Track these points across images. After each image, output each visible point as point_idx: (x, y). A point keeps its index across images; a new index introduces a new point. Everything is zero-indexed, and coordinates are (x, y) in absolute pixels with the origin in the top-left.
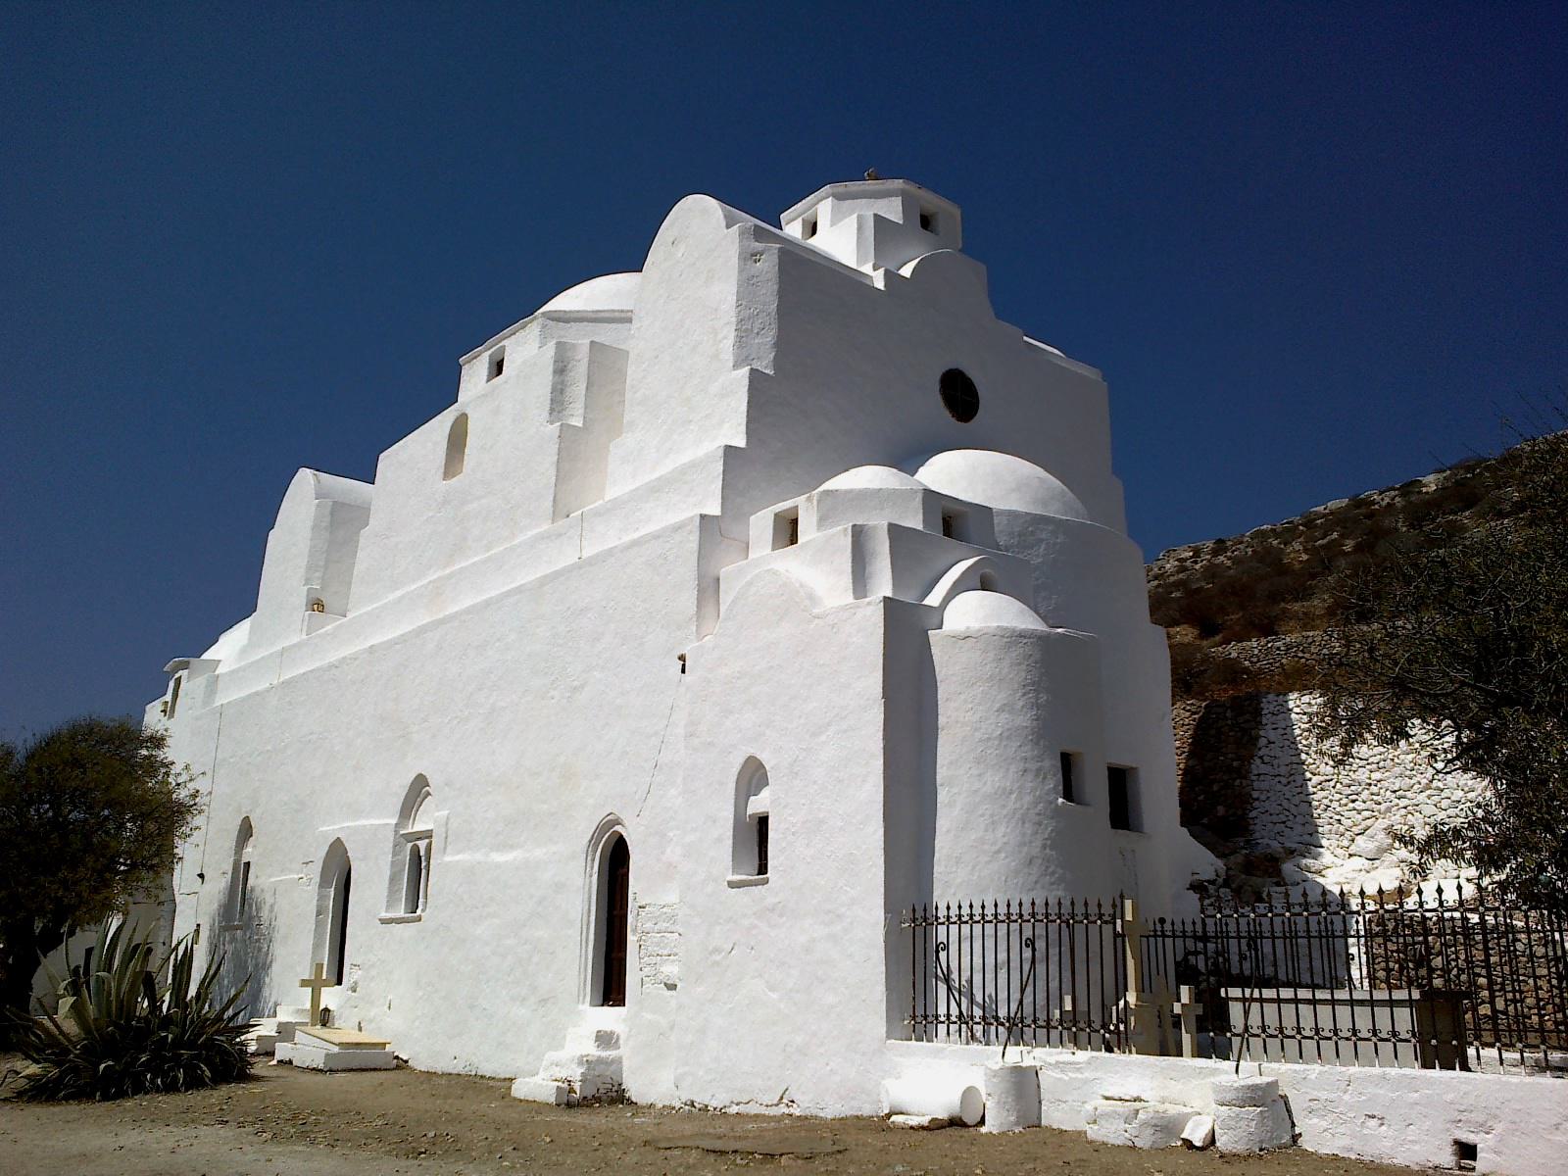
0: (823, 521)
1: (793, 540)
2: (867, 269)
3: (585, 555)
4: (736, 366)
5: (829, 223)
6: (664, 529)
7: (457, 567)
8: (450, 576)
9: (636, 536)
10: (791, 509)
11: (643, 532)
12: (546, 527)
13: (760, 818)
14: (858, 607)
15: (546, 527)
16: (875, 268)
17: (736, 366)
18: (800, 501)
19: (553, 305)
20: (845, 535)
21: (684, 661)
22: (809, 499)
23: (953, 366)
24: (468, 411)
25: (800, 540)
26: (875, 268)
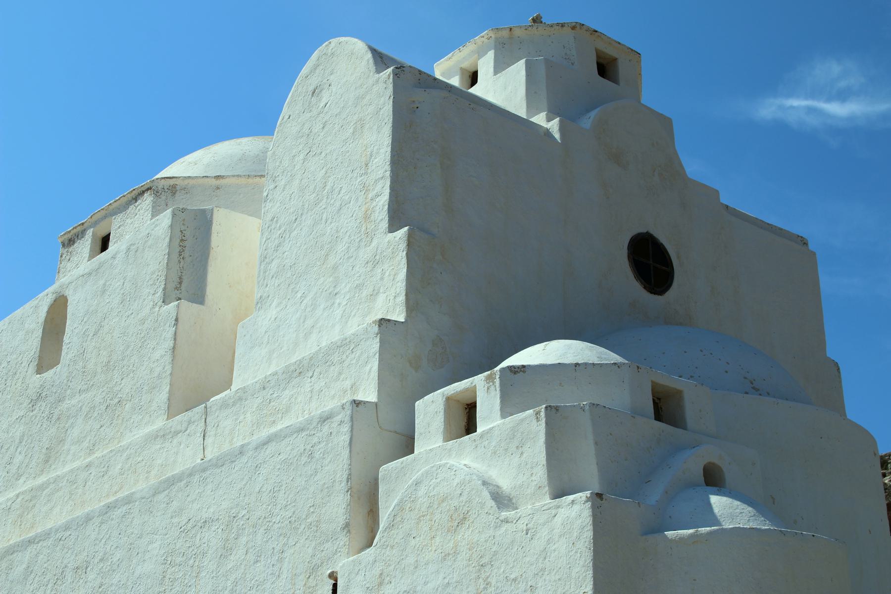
0: (508, 407)
1: (470, 427)
2: (540, 119)
3: (209, 456)
4: (393, 228)
5: (492, 70)
6: (309, 421)
7: (53, 475)
8: (42, 487)
9: (273, 430)
10: (466, 390)
11: (279, 427)
12: (160, 423)
13: (468, 405)
14: (559, 507)
15: (160, 423)
16: (549, 120)
17: (393, 228)
18: (479, 380)
19: (378, 354)
20: (538, 419)
21: (336, 580)
22: (490, 379)
23: (643, 230)
24: (69, 293)
25: (480, 429)
26: (549, 120)
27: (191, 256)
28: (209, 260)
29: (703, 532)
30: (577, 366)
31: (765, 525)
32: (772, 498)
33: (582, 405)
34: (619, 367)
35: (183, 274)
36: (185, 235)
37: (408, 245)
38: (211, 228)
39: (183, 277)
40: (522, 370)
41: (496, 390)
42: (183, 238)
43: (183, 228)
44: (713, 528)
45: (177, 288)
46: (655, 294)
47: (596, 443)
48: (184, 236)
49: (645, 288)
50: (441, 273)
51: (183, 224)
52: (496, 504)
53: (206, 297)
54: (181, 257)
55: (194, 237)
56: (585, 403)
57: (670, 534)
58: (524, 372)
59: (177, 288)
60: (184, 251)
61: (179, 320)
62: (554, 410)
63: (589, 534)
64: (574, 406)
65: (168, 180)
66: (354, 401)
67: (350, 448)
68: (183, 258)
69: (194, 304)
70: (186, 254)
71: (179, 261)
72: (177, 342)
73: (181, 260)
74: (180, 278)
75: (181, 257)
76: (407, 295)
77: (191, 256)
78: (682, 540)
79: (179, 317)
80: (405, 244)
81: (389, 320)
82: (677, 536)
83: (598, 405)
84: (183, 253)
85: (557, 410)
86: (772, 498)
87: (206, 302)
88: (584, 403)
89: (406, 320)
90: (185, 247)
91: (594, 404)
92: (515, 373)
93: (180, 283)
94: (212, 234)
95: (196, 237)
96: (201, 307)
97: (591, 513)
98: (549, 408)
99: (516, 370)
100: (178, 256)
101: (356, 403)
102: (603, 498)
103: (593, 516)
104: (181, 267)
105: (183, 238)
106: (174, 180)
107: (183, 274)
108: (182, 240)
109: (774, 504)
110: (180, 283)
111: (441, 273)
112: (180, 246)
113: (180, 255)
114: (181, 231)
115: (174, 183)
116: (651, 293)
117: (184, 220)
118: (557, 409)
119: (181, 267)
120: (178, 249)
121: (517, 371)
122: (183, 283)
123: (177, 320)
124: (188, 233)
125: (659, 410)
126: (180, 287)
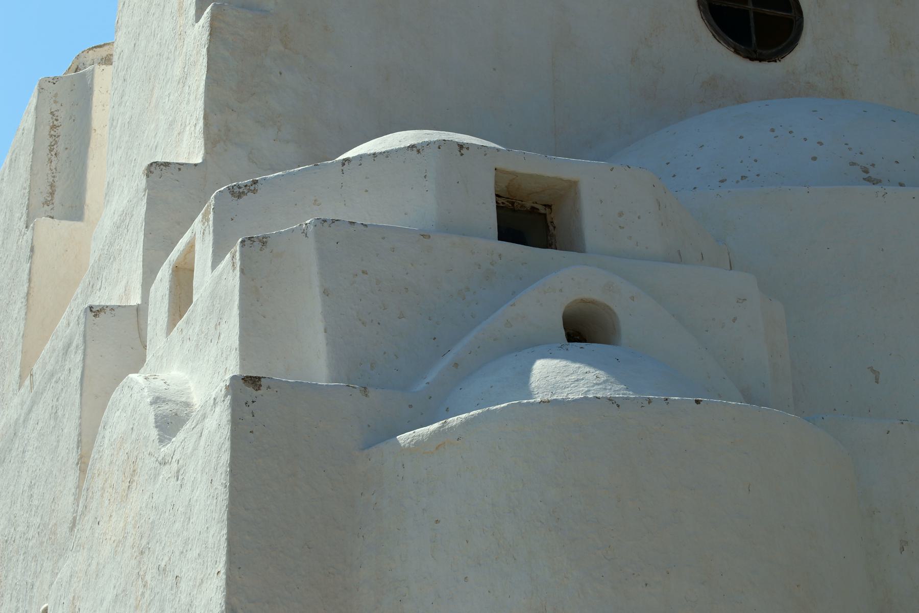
27: (66, 149)
28: (90, 149)
29: (455, 423)
30: (346, 163)
31: (616, 390)
32: (873, 371)
33: (304, 226)
34: (418, 151)
35: (56, 179)
36: (58, 118)
37: (210, 34)
38: (92, 99)
39: (56, 184)
40: (252, 188)
41: (210, 233)
42: (55, 123)
43: (54, 107)
44: (472, 413)
45: (46, 203)
46: (760, 61)
47: (326, 292)
48: (57, 120)
49: (737, 52)
50: (281, 74)
51: (55, 102)
52: (159, 435)
53: (86, 207)
54: (53, 153)
55: (71, 118)
56: (308, 222)
57: (404, 438)
58: (254, 191)
59: (46, 203)
60: (56, 142)
61: (36, 250)
62: (257, 245)
63: (226, 457)
64: (293, 230)
65: (98, 49)
66: (91, 308)
67: (81, 390)
68: (56, 154)
69: (63, 222)
70: (60, 148)
71: (49, 159)
72: (32, 285)
73: (53, 158)
74: (52, 186)
75: (53, 153)
76: (206, 118)
77: (66, 149)
78: (419, 444)
79: (35, 243)
80: (208, 33)
81: (167, 164)
82: (412, 441)
83: (333, 221)
84: (55, 146)
85: (264, 243)
86: (873, 371)
87: (87, 213)
88: (307, 222)
89: (205, 160)
90: (59, 136)
91: (325, 221)
92: (240, 196)
93: (52, 194)
94: (94, 108)
95: (73, 118)
96: (78, 224)
97: (230, 417)
98: (248, 242)
99: (241, 190)
100: (48, 152)
101: (94, 310)
102: (260, 385)
103: (232, 423)
104: (53, 168)
105: (55, 123)
106: (106, 48)
107: (56, 179)
108: (53, 127)
109: (877, 382)
110: (51, 194)
111: (281, 74)
112: (51, 136)
113: (51, 151)
114: (52, 113)
115: (107, 53)
116: (752, 59)
117: (56, 95)
118: (264, 241)
119: (53, 168)
120: (48, 141)
121: (243, 192)
122: (56, 193)
123: (32, 250)
124: (61, 115)
125: (548, 227)
126: (52, 200)
